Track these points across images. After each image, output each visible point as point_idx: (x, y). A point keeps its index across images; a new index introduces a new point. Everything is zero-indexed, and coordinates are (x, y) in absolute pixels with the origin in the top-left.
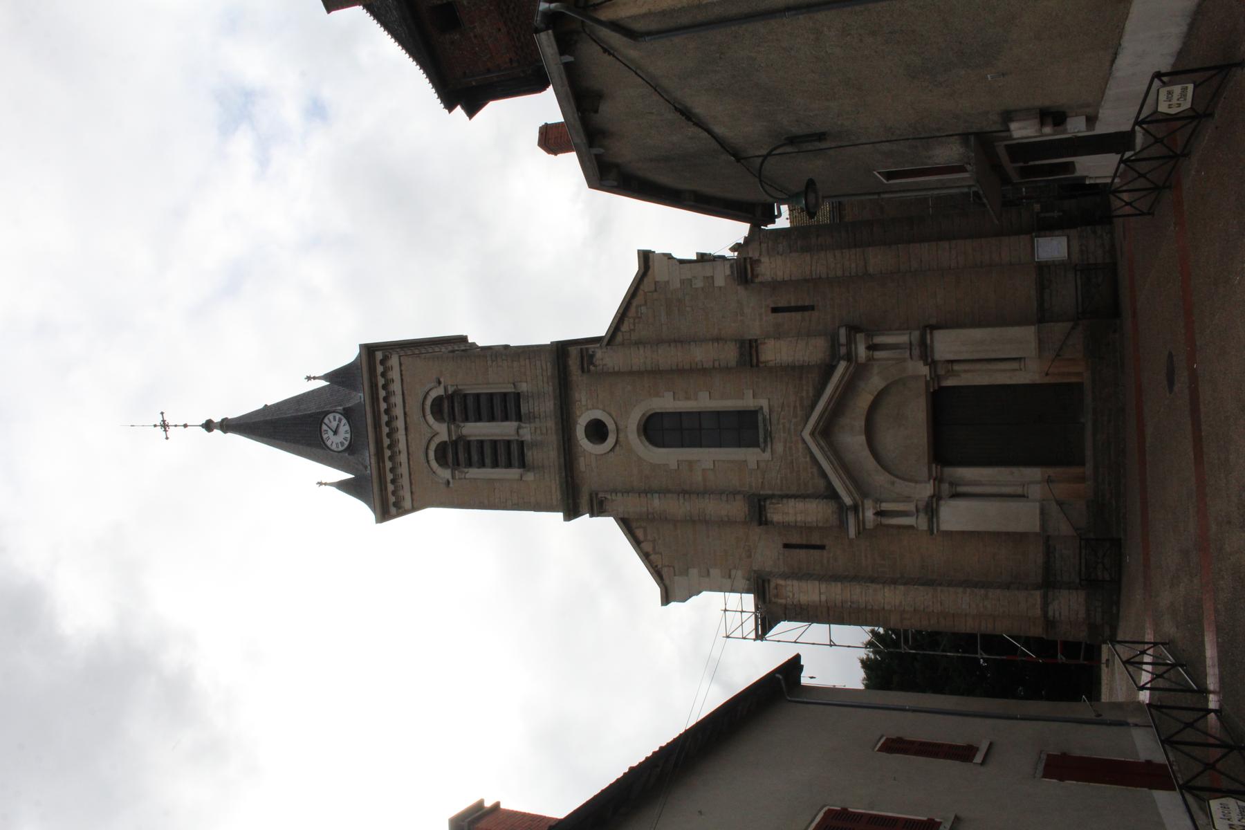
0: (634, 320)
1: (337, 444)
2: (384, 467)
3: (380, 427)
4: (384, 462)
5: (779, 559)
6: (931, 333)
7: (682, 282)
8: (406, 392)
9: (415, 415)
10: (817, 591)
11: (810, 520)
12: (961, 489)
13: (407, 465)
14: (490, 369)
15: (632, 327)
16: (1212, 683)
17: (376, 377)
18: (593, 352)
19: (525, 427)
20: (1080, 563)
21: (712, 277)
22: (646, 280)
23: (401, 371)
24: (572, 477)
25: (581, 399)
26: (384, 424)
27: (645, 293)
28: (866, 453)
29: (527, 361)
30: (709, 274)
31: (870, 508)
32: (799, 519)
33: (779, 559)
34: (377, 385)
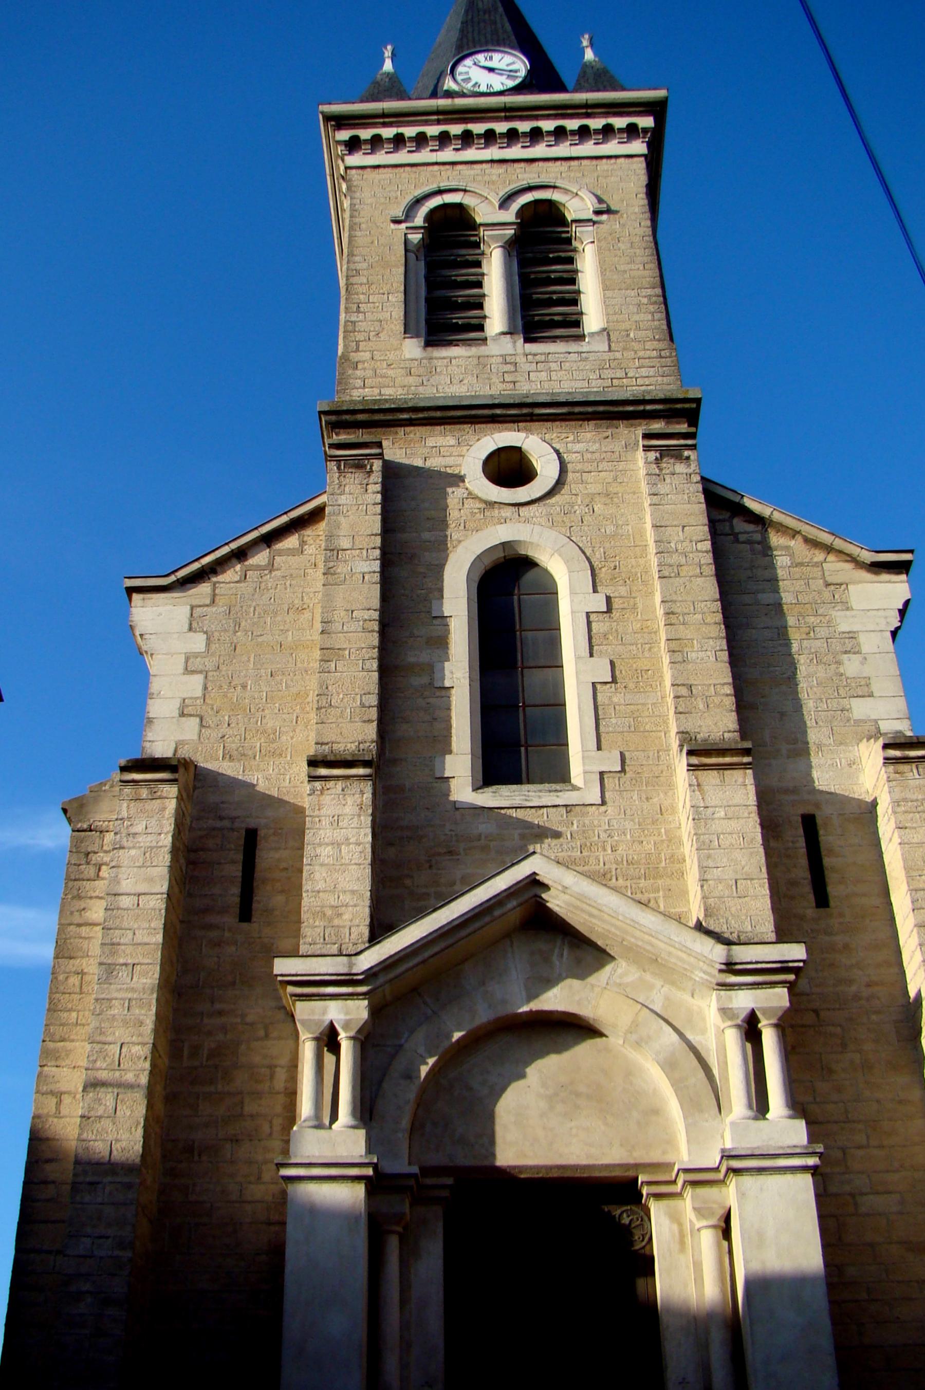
0: (759, 543)
1: (467, 73)
2: (427, 123)
3: (507, 119)
4: (438, 122)
5: (221, 818)
6: (804, 1169)
7: (852, 636)
8: (573, 163)
9: (528, 176)
10: (142, 888)
11: (317, 876)
12: (393, 1244)
13: (434, 160)
14: (633, 293)
15: (742, 538)
16: (648, 510)
17: (606, 115)
18: (688, 458)
19: (514, 346)
20: (593, 907)
21: (871, 695)
22: (849, 566)
23: (617, 157)
24: (411, 423)
25: (579, 442)
26: (514, 126)
27: (820, 564)
28: (483, 1015)
29: (655, 353)
30: (875, 687)
31: (347, 1013)
32: (496, 511)
33: (221, 818)
34: (588, 116)
